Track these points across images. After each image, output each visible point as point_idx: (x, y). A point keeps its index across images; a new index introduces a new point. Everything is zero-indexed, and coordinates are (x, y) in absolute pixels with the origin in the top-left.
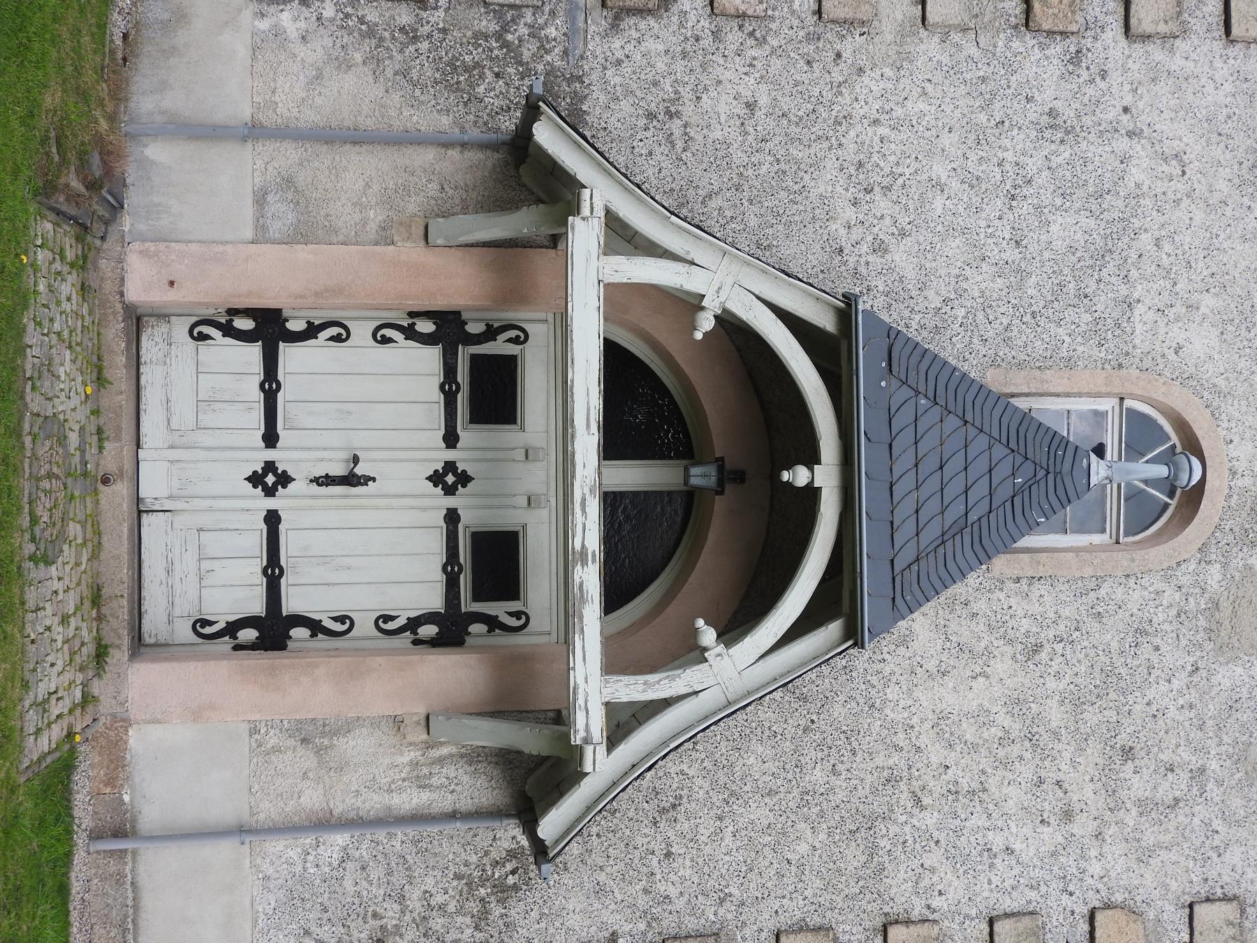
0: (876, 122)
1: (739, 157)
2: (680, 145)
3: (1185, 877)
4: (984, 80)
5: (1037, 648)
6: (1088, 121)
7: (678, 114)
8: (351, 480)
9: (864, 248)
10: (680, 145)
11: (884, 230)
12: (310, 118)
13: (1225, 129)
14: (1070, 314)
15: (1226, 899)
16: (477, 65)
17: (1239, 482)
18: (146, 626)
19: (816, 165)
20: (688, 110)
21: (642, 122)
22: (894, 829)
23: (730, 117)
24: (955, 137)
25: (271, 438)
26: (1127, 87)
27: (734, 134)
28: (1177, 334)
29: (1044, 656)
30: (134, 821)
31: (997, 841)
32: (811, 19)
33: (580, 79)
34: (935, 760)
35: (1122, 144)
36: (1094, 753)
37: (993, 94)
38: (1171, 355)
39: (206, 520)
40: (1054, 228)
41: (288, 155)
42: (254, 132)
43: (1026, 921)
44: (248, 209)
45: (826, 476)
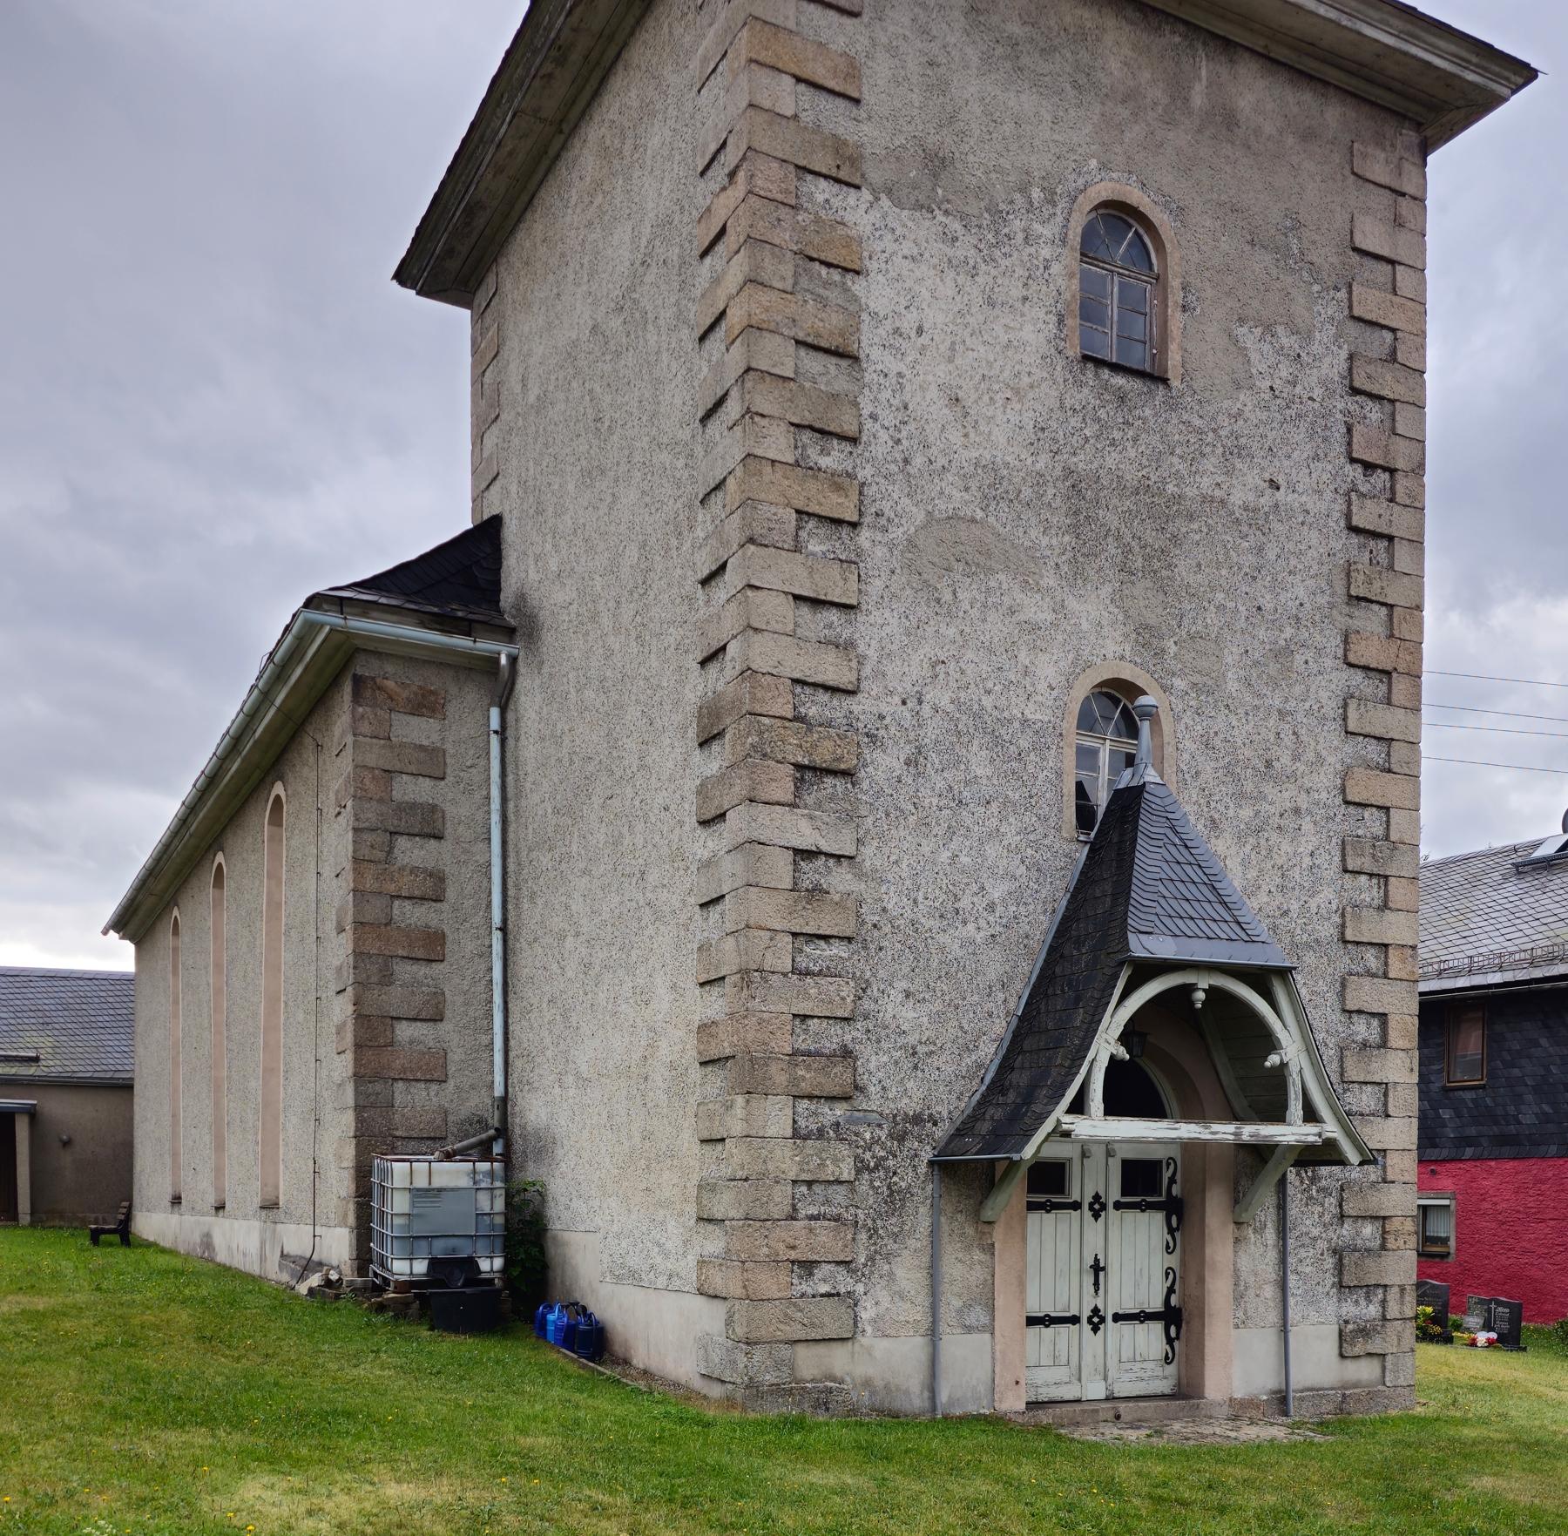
0: (915, 901)
1: (938, 1006)
2: (932, 1048)
3: (1331, 735)
4: (887, 815)
5: (1213, 821)
6: (912, 736)
7: (913, 1048)
8: (1097, 1268)
9: (991, 919)
10: (932, 1048)
11: (981, 904)
12: (923, 1299)
13: (914, 622)
14: (1030, 767)
15: (1345, 706)
16: (889, 1188)
17: (1128, 654)
18: (1167, 1391)
19: (942, 949)
20: (912, 1039)
21: (919, 1074)
22: (1298, 931)
23: (914, 1010)
24: (924, 842)
25: (1075, 1320)
26: (889, 699)
27: (927, 1007)
28: (1042, 687)
29: (1216, 816)
30: (1275, 1392)
31: (1307, 861)
32: (853, 946)
33: (895, 1116)
34: (1266, 899)
35: (926, 710)
36: (1269, 789)
37: (897, 809)
38: (1055, 693)
39: (1116, 1360)
40: (979, 773)
41: (947, 1314)
42: (933, 1334)
43: (1348, 848)
44: (975, 1337)
45: (1204, 982)
